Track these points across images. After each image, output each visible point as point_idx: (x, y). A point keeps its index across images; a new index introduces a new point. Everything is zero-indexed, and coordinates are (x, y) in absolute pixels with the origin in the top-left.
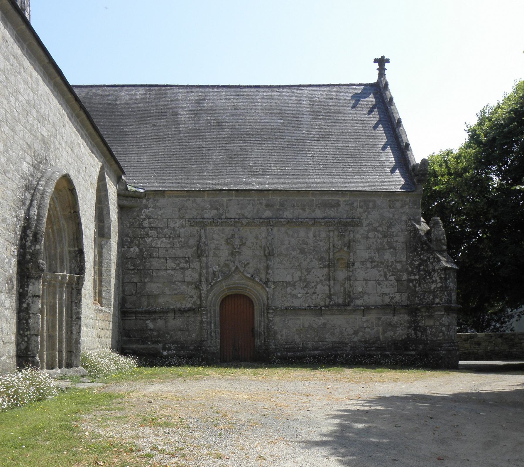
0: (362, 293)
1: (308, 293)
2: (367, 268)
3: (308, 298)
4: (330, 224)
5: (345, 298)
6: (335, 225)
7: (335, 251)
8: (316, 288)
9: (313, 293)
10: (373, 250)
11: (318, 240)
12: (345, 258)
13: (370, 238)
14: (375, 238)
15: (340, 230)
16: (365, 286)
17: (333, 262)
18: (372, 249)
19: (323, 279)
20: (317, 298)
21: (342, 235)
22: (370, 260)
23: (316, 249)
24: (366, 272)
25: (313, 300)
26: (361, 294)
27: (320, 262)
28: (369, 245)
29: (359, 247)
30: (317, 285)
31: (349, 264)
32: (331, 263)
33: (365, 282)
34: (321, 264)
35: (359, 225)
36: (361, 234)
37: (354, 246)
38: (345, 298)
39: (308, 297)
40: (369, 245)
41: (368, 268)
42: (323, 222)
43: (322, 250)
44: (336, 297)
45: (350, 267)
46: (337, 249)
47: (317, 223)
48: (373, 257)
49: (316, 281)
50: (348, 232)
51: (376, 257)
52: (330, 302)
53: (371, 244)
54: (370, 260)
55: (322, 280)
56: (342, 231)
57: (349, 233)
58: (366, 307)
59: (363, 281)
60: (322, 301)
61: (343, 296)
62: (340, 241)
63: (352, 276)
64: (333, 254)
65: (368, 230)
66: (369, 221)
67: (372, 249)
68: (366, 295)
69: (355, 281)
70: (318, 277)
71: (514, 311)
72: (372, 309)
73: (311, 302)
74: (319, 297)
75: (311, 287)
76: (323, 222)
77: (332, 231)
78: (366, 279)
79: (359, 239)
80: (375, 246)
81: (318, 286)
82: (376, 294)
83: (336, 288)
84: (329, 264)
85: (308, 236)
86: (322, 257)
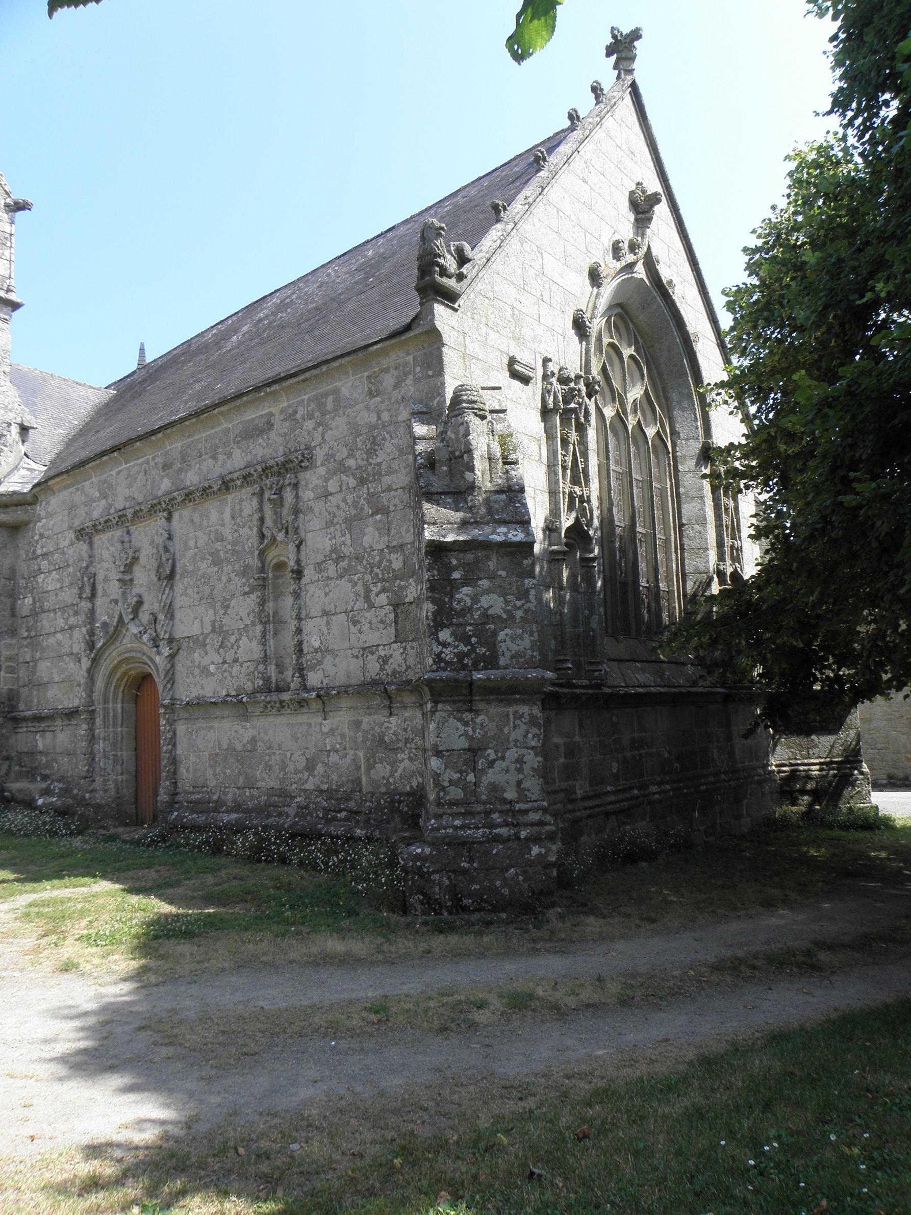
0: (321, 651)
2: (329, 578)
13: (331, 494)
14: (341, 491)
18: (338, 523)
22: (334, 556)
27: (244, 580)
40: (330, 514)
41: (332, 578)
53: (335, 509)
54: (334, 556)
80: (343, 514)
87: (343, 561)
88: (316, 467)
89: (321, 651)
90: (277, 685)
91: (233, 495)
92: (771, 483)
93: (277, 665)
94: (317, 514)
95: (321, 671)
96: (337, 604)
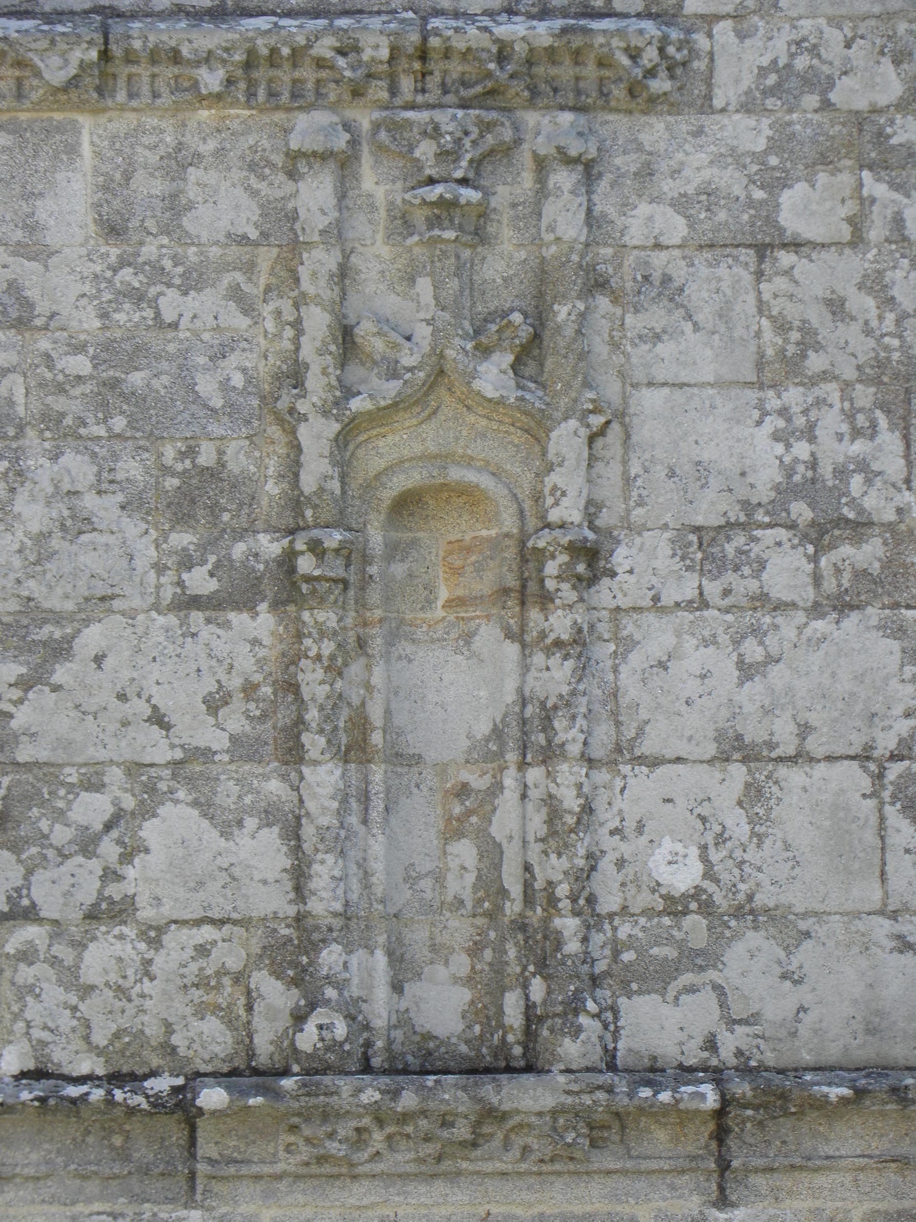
0: (707, 908)
1: (30, 914)
2: (761, 600)
3: (26, 973)
4: (308, 74)
5: (498, 967)
6: (357, 93)
7: (356, 404)
8: (127, 858)
9: (92, 915)
10: (831, 391)
11: (157, 273)
12: (486, 481)
13: (796, 245)
14: (857, 241)
15: (425, 150)
16: (739, 828)
17: (334, 538)
18: (825, 376)
19: (218, 741)
20: (146, 969)
21: (447, 205)
22: (801, 511)
23: (137, 379)
24: (753, 651)
25: (87, 990)
26: (695, 923)
27: (183, 539)
28: (782, 326)
29: (664, 349)
30: (146, 811)
31: (541, 556)
32: (315, 547)
33: (738, 772)
34: (187, 562)
35: (660, 85)
36: (681, 204)
37: (601, 349)
38: (498, 967)
39: (27, 956)
40: (782, 326)
41: (780, 607)
42: (208, 59)
43: (206, 386)
44: (381, 959)
45: (546, 599)
46: (393, 373)
47: (143, 71)
48: (841, 473)
49: (134, 768)
50: (528, 180)
51: (871, 476)
52: (299, 1018)
53: (816, 315)
54: (801, 511)
55: (206, 754)
56: (447, 155)
57: (542, 191)
58: (741, 1088)
59: (724, 758)
60: (201, 1011)
61: (475, 951)
62: (424, 286)
63: (567, 702)
64: (342, 441)
65: (773, 146)
66: (780, 48)
67: (825, 376)
68: (754, 939)
69: (612, 764)
70: (159, 719)
71: (604, 321)
72: (821, 1105)
73: (66, 1021)
74: (162, 962)
75: (61, 835)
76: (208, 59)
77: (324, 156)
78: (753, 732)
79: (659, 259)
80: (864, 347)
81: (150, 831)
82: (882, 927)
83: (377, 846)
84: (289, 558)
85: (32, 227)
86: (213, 474)
87: (858, 540)
88: (706, 105)
89: (707, 908)
90: (392, 1057)
91: (122, 123)
92: (888, 535)
93: (390, 954)
94: (704, 316)
95: (708, 999)
96: (813, 719)
